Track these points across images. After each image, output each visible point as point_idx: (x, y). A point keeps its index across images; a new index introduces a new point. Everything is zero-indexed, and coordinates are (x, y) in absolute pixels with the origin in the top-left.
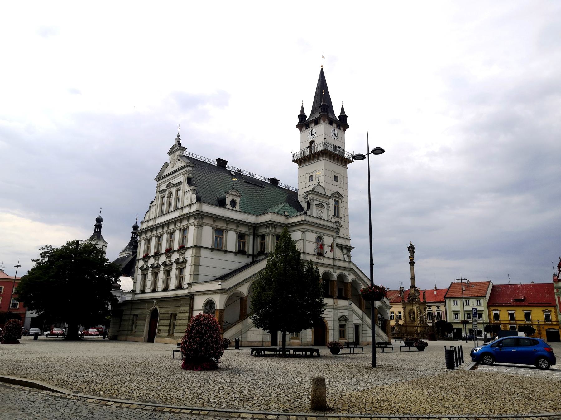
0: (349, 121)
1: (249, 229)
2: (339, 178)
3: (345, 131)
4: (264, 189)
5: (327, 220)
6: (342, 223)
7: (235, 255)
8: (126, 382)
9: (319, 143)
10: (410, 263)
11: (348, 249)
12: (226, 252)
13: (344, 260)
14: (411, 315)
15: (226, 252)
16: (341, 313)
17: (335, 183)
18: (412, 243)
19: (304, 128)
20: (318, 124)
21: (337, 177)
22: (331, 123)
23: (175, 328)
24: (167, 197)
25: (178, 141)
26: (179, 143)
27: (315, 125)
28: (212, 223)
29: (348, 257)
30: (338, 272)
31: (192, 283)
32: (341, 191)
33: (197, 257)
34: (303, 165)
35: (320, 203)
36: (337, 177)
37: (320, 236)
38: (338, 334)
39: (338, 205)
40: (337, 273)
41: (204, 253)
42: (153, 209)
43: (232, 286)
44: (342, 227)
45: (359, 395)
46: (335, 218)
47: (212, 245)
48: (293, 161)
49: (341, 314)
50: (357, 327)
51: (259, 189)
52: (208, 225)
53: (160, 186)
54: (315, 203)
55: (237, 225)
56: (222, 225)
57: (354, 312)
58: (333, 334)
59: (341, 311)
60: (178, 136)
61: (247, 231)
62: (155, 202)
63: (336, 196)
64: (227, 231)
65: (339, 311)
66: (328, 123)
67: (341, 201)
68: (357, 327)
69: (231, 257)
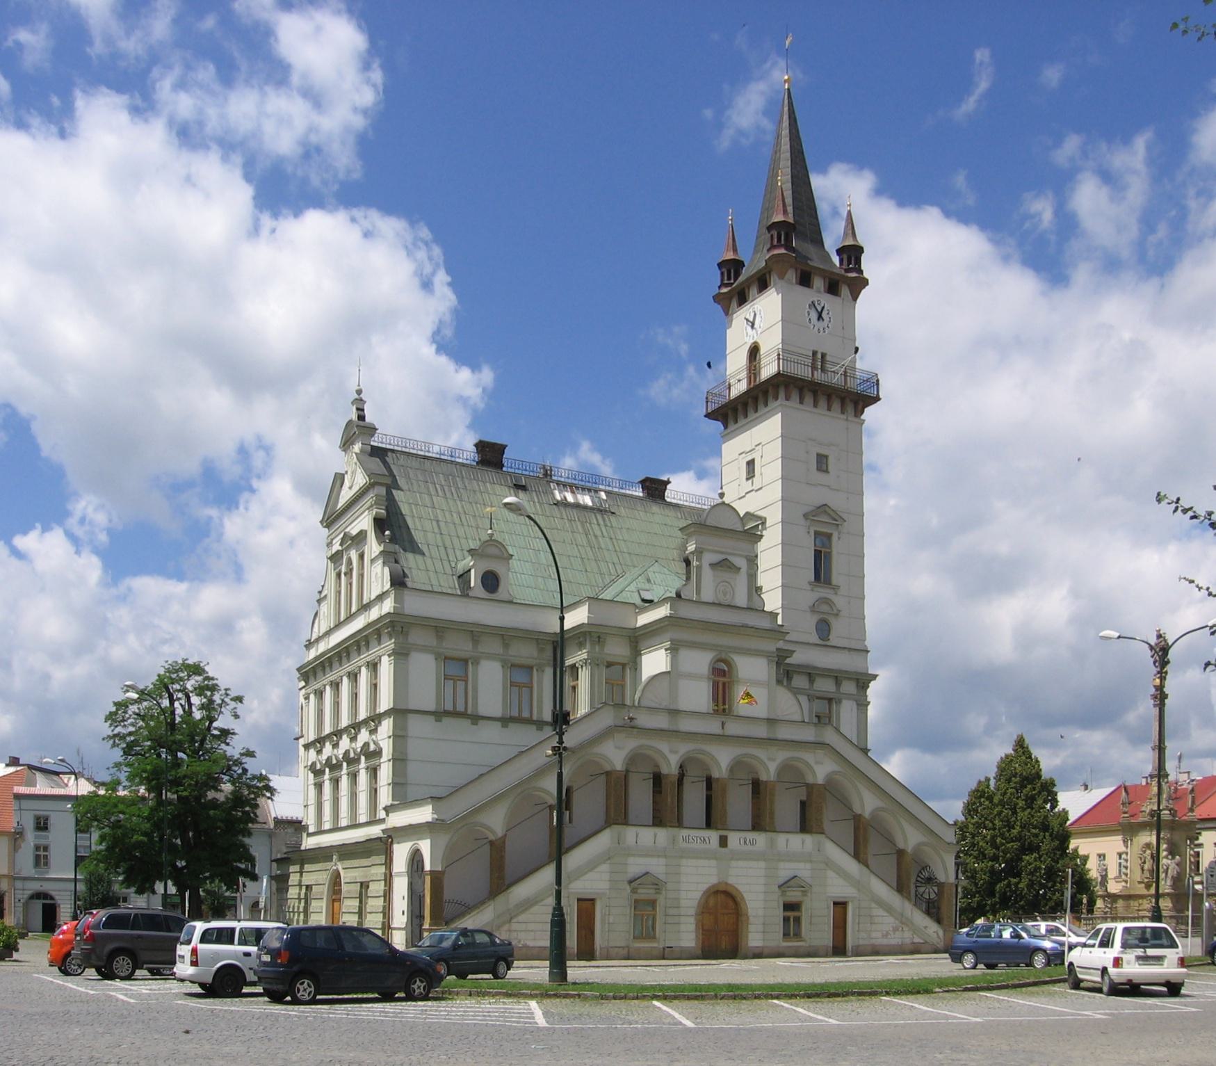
0: (868, 266)
1: (541, 650)
2: (831, 460)
3: (855, 298)
4: (613, 518)
5: (749, 609)
6: (840, 602)
7: (502, 727)
8: (398, 1052)
9: (359, 520)
10: (1154, 697)
11: (858, 680)
12: (476, 719)
13: (804, 722)
14: (1144, 862)
15: (476, 719)
16: (785, 871)
17: (821, 477)
18: (1161, 632)
19: (734, 303)
20: (746, 302)
21: (826, 457)
22: (805, 280)
23: (368, 919)
24: (345, 574)
25: (358, 409)
26: (361, 418)
27: (740, 305)
28: (434, 642)
29: (858, 704)
30: (781, 755)
31: (392, 805)
32: (837, 502)
33: (399, 737)
34: (732, 427)
35: (723, 557)
36: (826, 457)
37: (723, 656)
38: (779, 928)
39: (830, 547)
40: (779, 761)
41: (416, 726)
42: (324, 608)
43: (1158, 729)
44: (841, 613)
45: (424, 1052)
46: (816, 589)
47: (437, 704)
48: (708, 416)
49: (789, 874)
50: (840, 906)
51: (597, 520)
52: (424, 649)
53: (331, 543)
54: (709, 558)
55: (503, 643)
56: (459, 646)
57: (829, 863)
58: (760, 928)
59: (788, 865)
60: (359, 392)
61: (535, 654)
62: (326, 587)
63: (825, 519)
64: (476, 662)
65: (782, 865)
66: (794, 281)
67: (839, 533)
68: (840, 906)
69: (491, 732)
